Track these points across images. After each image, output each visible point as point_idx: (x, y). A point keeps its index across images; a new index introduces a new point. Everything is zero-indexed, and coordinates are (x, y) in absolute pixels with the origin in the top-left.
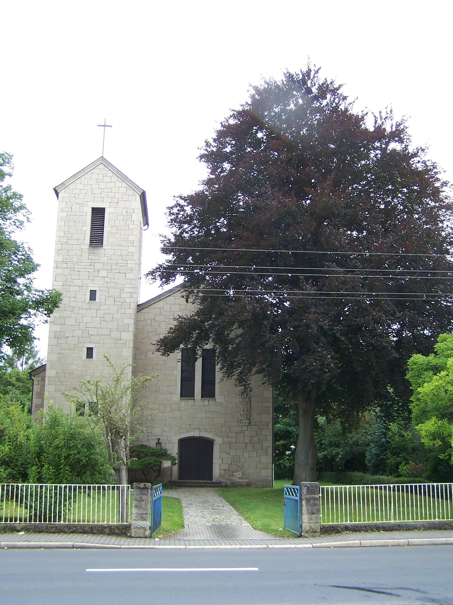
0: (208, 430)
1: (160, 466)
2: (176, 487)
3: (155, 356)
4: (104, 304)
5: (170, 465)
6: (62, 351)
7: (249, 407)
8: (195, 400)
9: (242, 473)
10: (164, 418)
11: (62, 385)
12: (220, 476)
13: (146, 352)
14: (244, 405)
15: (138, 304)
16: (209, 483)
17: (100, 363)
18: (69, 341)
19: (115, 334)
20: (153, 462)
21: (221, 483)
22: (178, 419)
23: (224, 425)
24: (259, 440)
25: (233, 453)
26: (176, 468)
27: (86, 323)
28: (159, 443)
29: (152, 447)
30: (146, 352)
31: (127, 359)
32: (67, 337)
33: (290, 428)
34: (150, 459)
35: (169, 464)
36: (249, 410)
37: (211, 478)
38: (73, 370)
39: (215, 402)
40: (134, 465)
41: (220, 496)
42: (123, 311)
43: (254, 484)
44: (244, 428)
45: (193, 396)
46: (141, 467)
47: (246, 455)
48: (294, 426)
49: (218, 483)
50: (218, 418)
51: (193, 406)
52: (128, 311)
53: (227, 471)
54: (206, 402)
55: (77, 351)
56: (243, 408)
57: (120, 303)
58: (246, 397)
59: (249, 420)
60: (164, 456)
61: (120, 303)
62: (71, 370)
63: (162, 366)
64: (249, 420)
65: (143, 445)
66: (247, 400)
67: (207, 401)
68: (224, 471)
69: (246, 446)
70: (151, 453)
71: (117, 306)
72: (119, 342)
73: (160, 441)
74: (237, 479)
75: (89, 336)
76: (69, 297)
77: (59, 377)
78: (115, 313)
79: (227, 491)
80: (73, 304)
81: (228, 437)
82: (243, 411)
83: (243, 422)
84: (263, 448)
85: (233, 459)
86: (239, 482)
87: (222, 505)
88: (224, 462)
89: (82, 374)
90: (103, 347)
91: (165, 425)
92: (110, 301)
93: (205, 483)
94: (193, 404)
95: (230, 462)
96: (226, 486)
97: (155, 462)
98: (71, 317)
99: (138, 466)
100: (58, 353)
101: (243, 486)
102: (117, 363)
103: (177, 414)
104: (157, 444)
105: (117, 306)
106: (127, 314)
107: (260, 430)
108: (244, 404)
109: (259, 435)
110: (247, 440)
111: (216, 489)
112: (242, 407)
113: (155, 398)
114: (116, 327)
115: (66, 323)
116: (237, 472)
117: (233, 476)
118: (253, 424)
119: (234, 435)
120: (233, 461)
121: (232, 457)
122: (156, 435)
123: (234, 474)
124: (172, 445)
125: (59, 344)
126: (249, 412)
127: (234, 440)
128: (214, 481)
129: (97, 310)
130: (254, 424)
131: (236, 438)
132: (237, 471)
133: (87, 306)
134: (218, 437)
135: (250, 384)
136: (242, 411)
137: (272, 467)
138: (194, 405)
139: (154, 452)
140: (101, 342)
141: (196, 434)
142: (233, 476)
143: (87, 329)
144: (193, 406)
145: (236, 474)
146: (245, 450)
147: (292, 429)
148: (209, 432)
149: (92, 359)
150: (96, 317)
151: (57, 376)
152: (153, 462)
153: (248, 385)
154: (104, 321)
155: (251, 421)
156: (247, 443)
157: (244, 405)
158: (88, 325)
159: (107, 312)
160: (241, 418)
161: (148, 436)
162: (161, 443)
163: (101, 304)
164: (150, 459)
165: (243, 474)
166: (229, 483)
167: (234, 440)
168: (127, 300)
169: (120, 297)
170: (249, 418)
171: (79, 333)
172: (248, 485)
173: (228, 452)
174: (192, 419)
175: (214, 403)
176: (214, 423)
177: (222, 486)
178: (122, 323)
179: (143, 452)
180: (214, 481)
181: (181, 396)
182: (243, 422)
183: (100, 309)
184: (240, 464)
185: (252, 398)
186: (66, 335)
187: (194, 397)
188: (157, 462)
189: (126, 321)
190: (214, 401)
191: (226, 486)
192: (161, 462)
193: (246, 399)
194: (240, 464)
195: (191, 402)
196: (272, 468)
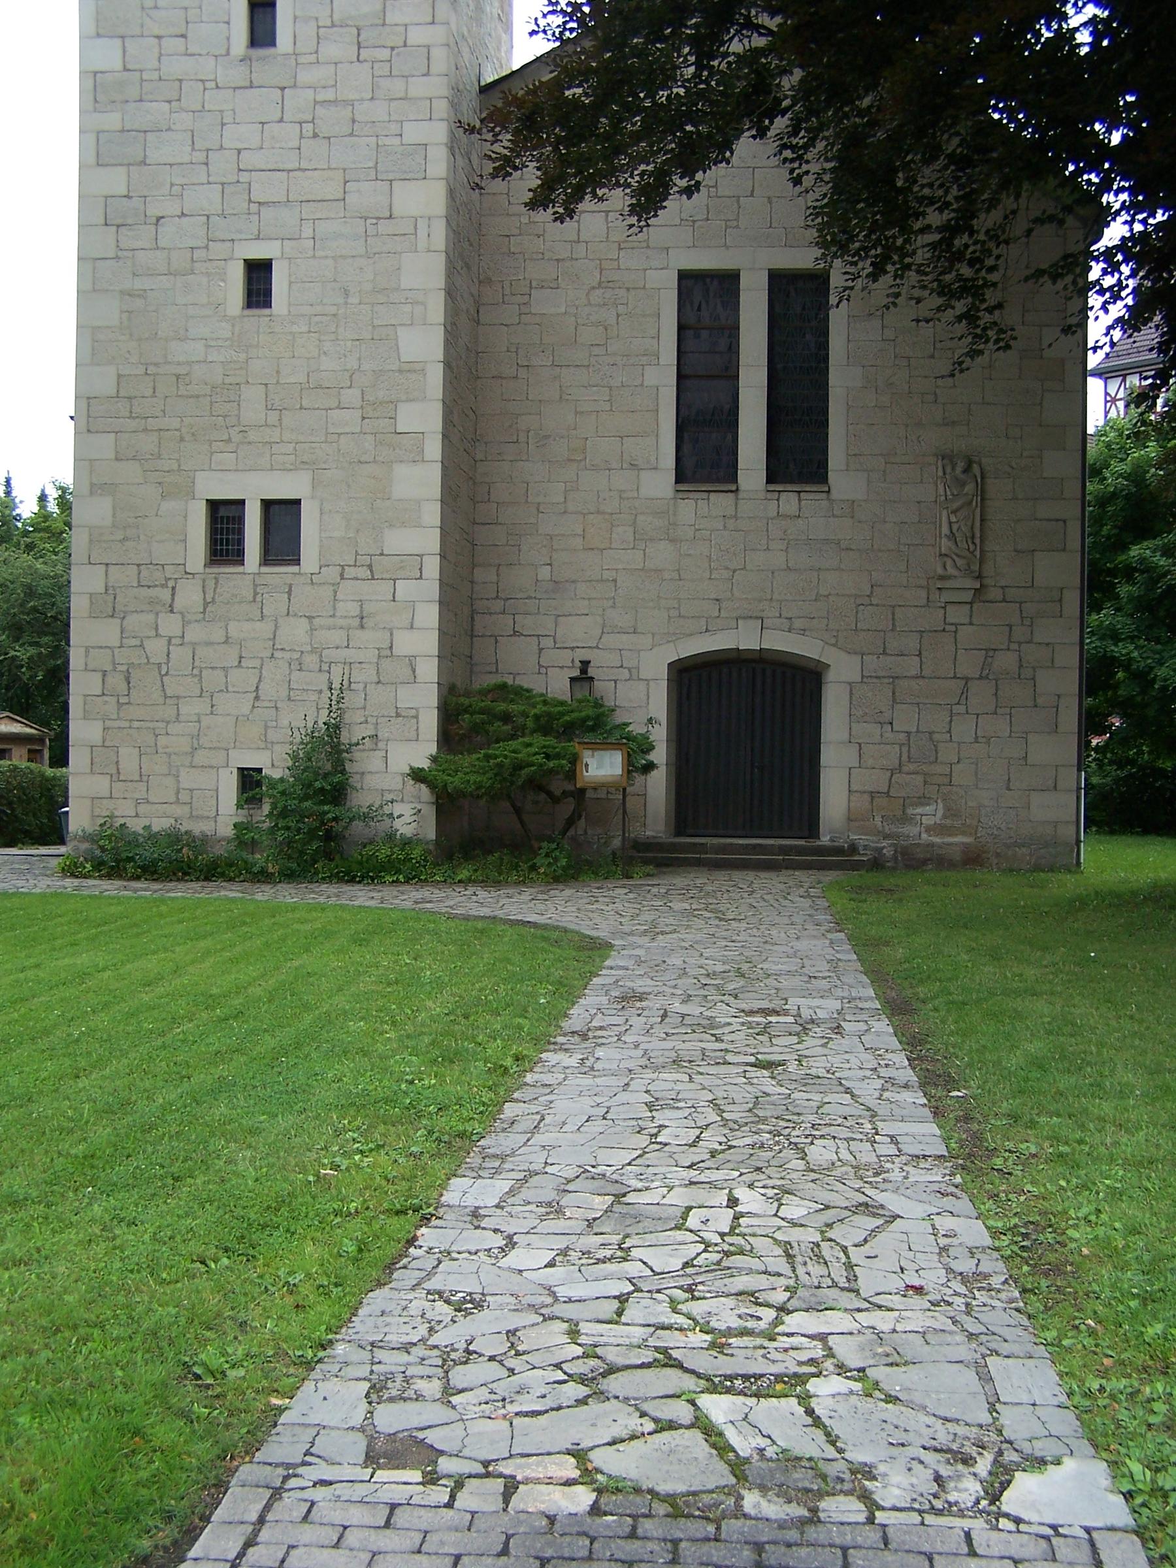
0: (798, 624)
1: (571, 775)
2: (650, 869)
3: (563, 310)
4: (313, 58)
5: (618, 771)
6: (139, 284)
7: (978, 524)
8: (741, 495)
9: (947, 809)
10: (607, 575)
11: (145, 430)
12: (849, 820)
13: (527, 290)
14: (954, 512)
15: (483, 83)
16: (800, 851)
17: (305, 329)
18: (168, 231)
19: (365, 195)
20: (540, 759)
21: (853, 849)
22: (666, 575)
23: (866, 601)
24: (1021, 666)
25: (906, 720)
26: (658, 784)
27: (239, 151)
28: (583, 676)
29: (561, 698)
30: (527, 290)
31: (422, 304)
32: (159, 219)
33: (1116, 645)
34: (529, 745)
35: (612, 765)
36: (978, 535)
37: (810, 825)
38: (189, 363)
39: (828, 499)
40: (456, 771)
41: (839, 926)
42: (398, 87)
43: (998, 855)
44: (957, 615)
45: (731, 475)
46: (485, 780)
47: (964, 729)
48: (1132, 638)
49: (838, 851)
50: (839, 569)
51: (731, 517)
52: (420, 87)
53: (881, 801)
54: (789, 501)
55: (205, 280)
56: (950, 523)
57: (385, 54)
58: (962, 476)
59: (980, 577)
60: (592, 729)
61: (385, 54)
62: (179, 364)
63: (596, 351)
64: (980, 577)
65: (503, 687)
66: (969, 488)
67: (794, 496)
68: (866, 797)
69: (965, 691)
70: (537, 718)
71: (367, 66)
72: (384, 227)
73: (591, 672)
74: (924, 836)
75: (254, 207)
76: (159, 37)
77: (129, 398)
78: (362, 100)
79: (880, 890)
80: (176, 67)
81: (884, 653)
82: (952, 536)
83: (948, 584)
84: (1040, 701)
85: (905, 749)
86: (932, 845)
87: (827, 1007)
88: (870, 762)
89: (227, 380)
90: (314, 256)
91: (610, 603)
92: (338, 48)
93: (784, 850)
94: (730, 511)
95: (897, 762)
96: (876, 864)
97: (548, 757)
98: (169, 129)
99: (473, 778)
100: (122, 292)
101: (952, 865)
102: (376, 322)
103: (662, 554)
104: (577, 685)
105: (367, 66)
106: (416, 99)
107: (1027, 622)
108: (955, 505)
109: (1020, 643)
110: (968, 666)
111: (831, 876)
112: (944, 519)
113: (566, 491)
114: (371, 164)
115: (153, 156)
116: (922, 805)
117: (905, 819)
118: (994, 593)
119: (912, 643)
120: (905, 757)
121: (902, 736)
122: (573, 648)
123: (910, 811)
124: (642, 686)
125: (125, 253)
126: (977, 541)
127: (912, 666)
128: (825, 840)
129: (283, 89)
130: (1000, 598)
131: (920, 655)
132: (923, 800)
133: (238, 75)
134: (843, 655)
135: (1000, 306)
136: (944, 540)
137: (1079, 782)
138: (736, 517)
139: (549, 714)
140: (307, 231)
141: (747, 639)
142: (905, 819)
143: (244, 177)
144: (731, 517)
145: (919, 810)
146: (962, 709)
147: (1124, 652)
148: (803, 631)
149: (266, 311)
150: (281, 120)
151: (122, 394)
152: (540, 759)
153: (990, 310)
154: (315, 136)
155: (987, 581)
156: (967, 679)
157: (954, 512)
158: (248, 159)
159: (329, 95)
160: (940, 571)
161: (541, 650)
162: (592, 679)
163: (301, 60)
164: (529, 745)
165: (950, 812)
166: (888, 852)
167: (912, 666)
168: (417, 36)
169: (384, 25)
170: (976, 567)
171: (206, 198)
172: (973, 859)
173: (887, 716)
174: (726, 574)
175: (825, 503)
176: (823, 592)
177: (855, 866)
178: (397, 141)
179: (506, 718)
180: (825, 840)
181: (679, 479)
182: (948, 584)
183: (295, 86)
184: (938, 769)
185: (988, 481)
186: (153, 212)
187: (734, 479)
188: (558, 756)
189: (414, 133)
190: (824, 495)
191: (876, 864)
192: (575, 760)
193: (963, 484)
194: (938, 769)
195: (721, 502)
196: (1079, 788)
